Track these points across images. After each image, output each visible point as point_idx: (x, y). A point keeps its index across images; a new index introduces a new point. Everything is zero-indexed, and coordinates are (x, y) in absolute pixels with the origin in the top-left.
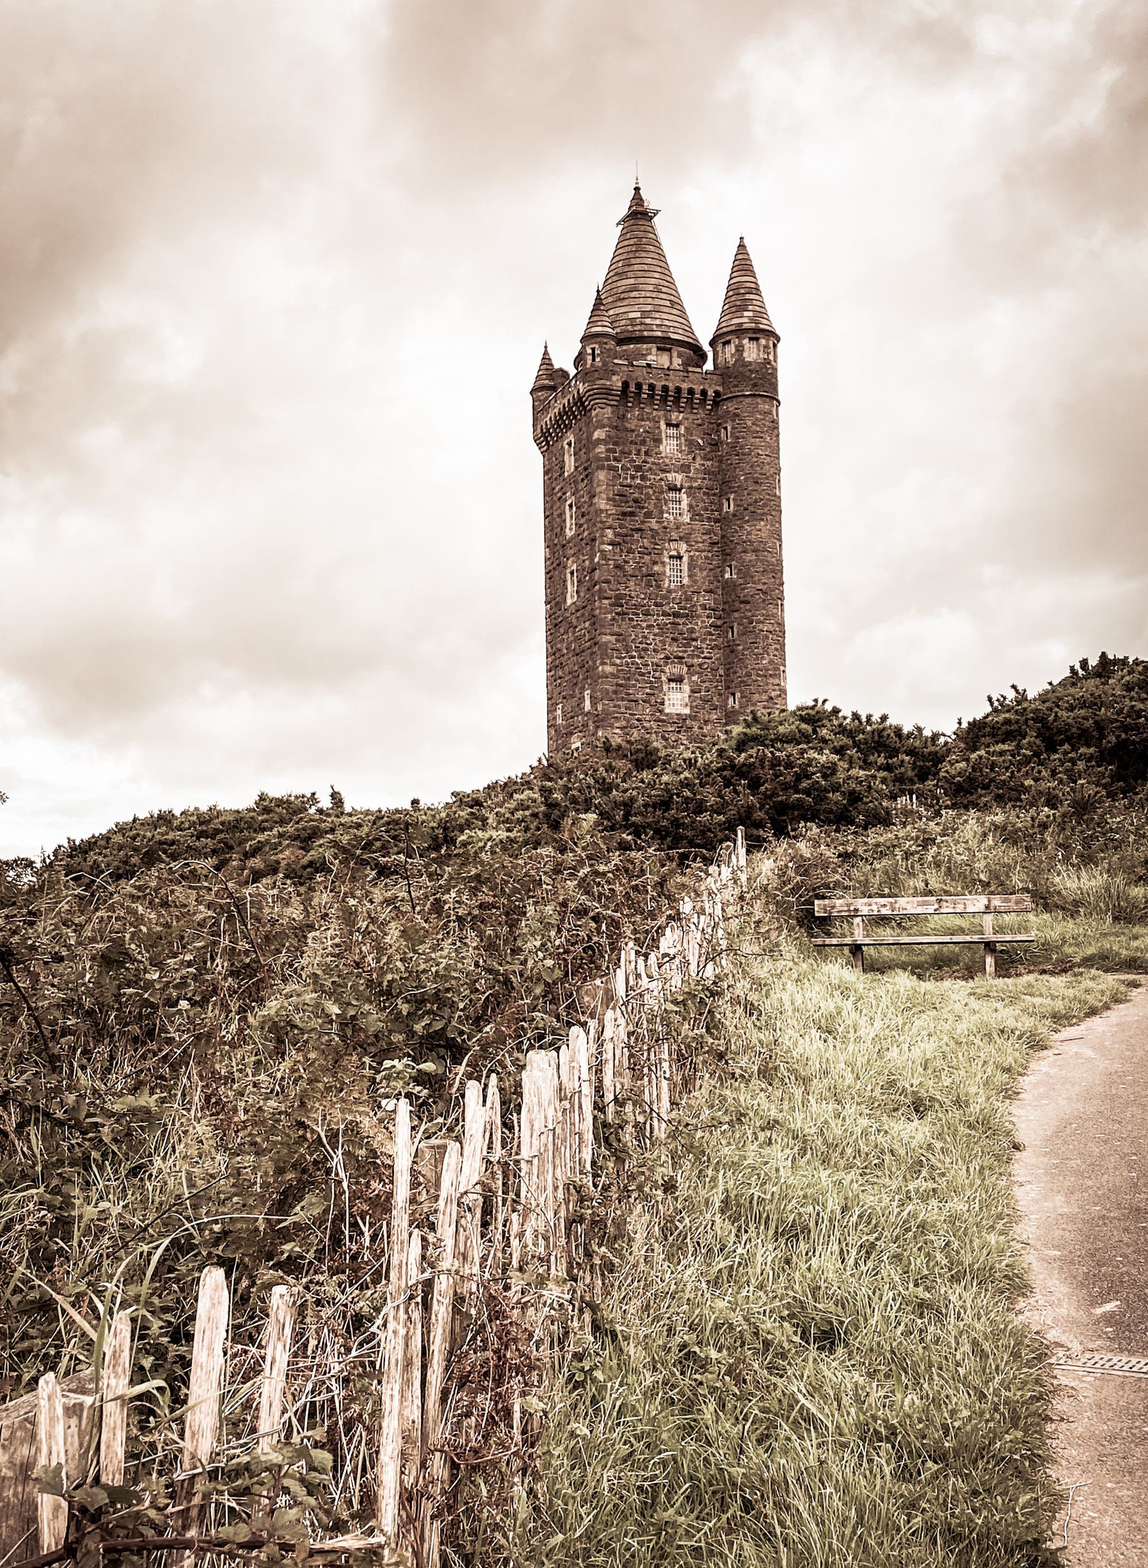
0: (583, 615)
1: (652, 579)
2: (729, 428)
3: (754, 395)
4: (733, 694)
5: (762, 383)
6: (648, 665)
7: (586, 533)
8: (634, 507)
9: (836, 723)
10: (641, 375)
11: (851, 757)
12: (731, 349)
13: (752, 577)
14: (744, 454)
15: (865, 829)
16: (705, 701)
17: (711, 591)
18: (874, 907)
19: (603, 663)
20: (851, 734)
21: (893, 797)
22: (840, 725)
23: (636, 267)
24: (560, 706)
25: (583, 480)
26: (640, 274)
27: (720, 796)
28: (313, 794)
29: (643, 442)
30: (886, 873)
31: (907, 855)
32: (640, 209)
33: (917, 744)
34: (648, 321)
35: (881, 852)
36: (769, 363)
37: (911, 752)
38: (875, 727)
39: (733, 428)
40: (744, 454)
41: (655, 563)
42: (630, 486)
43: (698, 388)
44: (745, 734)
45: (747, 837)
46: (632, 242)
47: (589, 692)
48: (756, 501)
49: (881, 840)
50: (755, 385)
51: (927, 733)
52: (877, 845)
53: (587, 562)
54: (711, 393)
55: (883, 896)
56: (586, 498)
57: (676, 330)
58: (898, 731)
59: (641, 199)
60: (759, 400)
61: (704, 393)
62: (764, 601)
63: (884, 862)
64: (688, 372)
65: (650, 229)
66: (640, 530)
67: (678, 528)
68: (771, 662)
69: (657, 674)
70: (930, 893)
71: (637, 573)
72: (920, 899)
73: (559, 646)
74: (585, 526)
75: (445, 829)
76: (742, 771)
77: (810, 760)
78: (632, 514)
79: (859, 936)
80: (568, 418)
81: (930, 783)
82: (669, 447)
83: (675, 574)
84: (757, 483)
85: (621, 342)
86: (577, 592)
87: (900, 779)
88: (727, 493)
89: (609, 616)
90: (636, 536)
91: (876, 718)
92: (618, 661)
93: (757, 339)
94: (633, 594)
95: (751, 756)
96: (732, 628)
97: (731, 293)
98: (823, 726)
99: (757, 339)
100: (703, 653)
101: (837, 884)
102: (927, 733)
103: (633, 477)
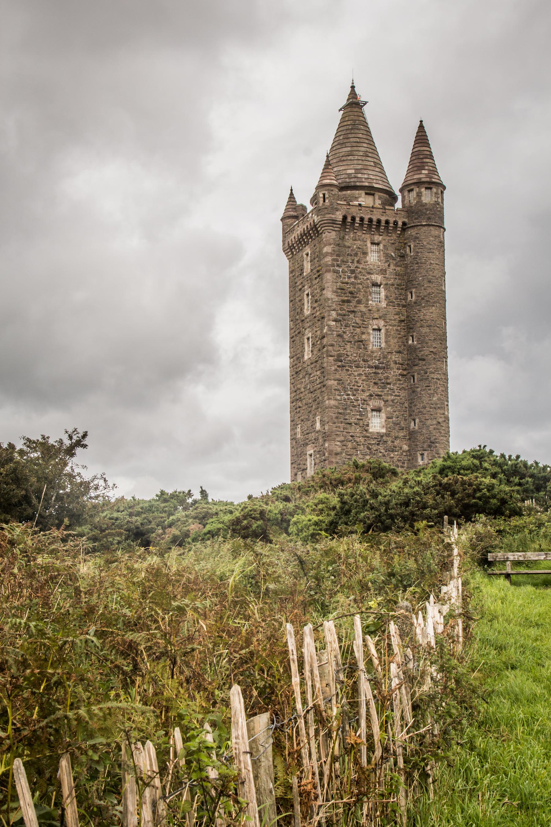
0: (315, 367)
1: (362, 343)
2: (412, 246)
3: (429, 225)
4: (414, 420)
5: (433, 217)
6: (358, 400)
7: (318, 313)
8: (349, 297)
9: (492, 459)
10: (354, 211)
11: (501, 478)
12: (414, 194)
13: (427, 343)
14: (421, 263)
15: (509, 517)
16: (396, 424)
17: (399, 352)
18: (516, 557)
19: (329, 399)
20: (500, 466)
21: (523, 500)
22: (494, 461)
23: (352, 140)
24: (299, 426)
25: (316, 278)
26: (355, 144)
27: (435, 500)
28: (190, 491)
29: (356, 255)
30: (521, 540)
31: (531, 532)
32: (354, 100)
33: (535, 471)
34: (360, 175)
35: (518, 530)
36: (438, 204)
37: (532, 476)
38: (513, 462)
39: (415, 246)
40: (421, 263)
41: (363, 333)
42: (347, 283)
43: (392, 220)
44: (444, 465)
45: (457, 524)
46: (349, 123)
47: (319, 417)
48: (429, 294)
49: (518, 523)
50: (429, 218)
51: (541, 465)
52: (516, 526)
53: (319, 332)
54: (400, 224)
55: (519, 552)
56: (318, 291)
57: (377, 182)
58: (525, 464)
59: (356, 94)
60: (431, 228)
61: (396, 223)
62: (435, 359)
63: (519, 535)
64: (385, 209)
65: (361, 114)
66: (353, 312)
67: (378, 310)
68: (439, 399)
69: (364, 406)
70: (542, 550)
71: (352, 340)
72: (537, 553)
73: (299, 386)
74: (318, 308)
75: (281, 514)
76: (447, 487)
77: (481, 482)
78: (348, 301)
79: (509, 570)
80: (307, 237)
81: (542, 493)
82: (373, 257)
83: (376, 341)
84: (430, 282)
85: (342, 189)
86: (312, 351)
87: (526, 491)
88: (410, 288)
89: (333, 368)
90: (352, 316)
91: (514, 457)
92: (339, 398)
93: (431, 188)
94: (349, 353)
95: (450, 479)
96: (413, 377)
97: (414, 158)
98: (485, 461)
99: (431, 188)
100: (394, 392)
101: (496, 546)
102: (541, 465)
103: (349, 277)
